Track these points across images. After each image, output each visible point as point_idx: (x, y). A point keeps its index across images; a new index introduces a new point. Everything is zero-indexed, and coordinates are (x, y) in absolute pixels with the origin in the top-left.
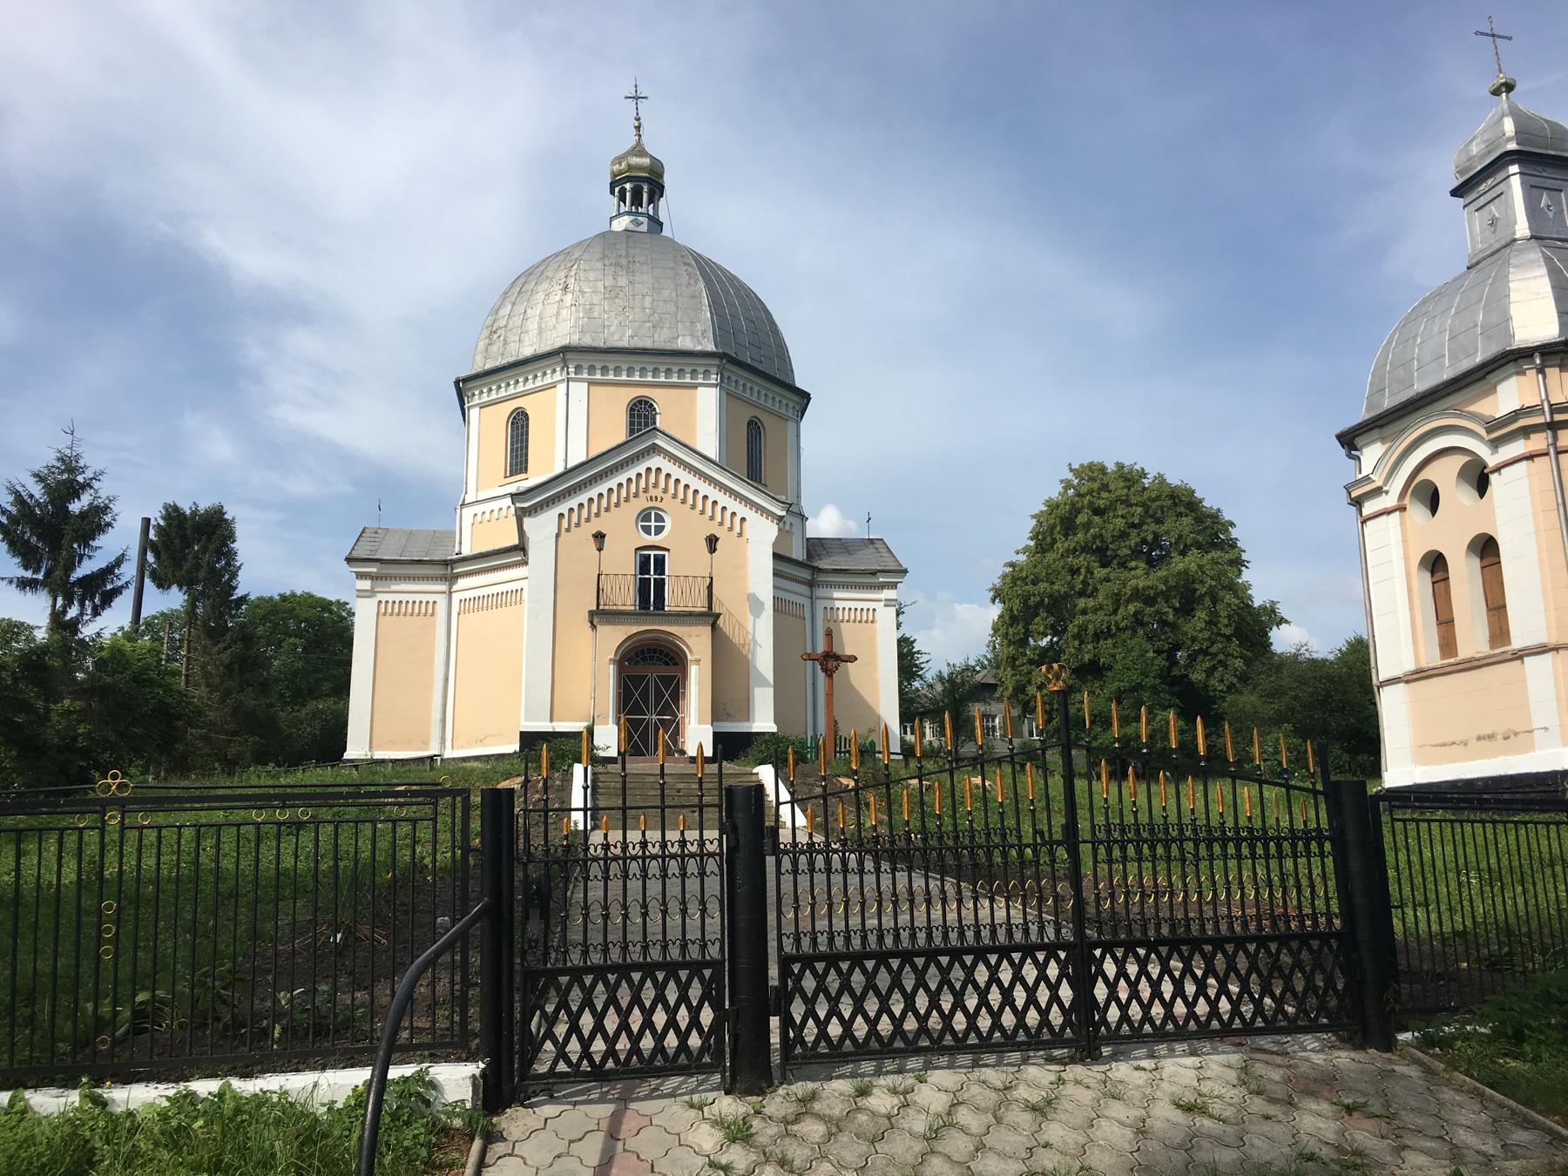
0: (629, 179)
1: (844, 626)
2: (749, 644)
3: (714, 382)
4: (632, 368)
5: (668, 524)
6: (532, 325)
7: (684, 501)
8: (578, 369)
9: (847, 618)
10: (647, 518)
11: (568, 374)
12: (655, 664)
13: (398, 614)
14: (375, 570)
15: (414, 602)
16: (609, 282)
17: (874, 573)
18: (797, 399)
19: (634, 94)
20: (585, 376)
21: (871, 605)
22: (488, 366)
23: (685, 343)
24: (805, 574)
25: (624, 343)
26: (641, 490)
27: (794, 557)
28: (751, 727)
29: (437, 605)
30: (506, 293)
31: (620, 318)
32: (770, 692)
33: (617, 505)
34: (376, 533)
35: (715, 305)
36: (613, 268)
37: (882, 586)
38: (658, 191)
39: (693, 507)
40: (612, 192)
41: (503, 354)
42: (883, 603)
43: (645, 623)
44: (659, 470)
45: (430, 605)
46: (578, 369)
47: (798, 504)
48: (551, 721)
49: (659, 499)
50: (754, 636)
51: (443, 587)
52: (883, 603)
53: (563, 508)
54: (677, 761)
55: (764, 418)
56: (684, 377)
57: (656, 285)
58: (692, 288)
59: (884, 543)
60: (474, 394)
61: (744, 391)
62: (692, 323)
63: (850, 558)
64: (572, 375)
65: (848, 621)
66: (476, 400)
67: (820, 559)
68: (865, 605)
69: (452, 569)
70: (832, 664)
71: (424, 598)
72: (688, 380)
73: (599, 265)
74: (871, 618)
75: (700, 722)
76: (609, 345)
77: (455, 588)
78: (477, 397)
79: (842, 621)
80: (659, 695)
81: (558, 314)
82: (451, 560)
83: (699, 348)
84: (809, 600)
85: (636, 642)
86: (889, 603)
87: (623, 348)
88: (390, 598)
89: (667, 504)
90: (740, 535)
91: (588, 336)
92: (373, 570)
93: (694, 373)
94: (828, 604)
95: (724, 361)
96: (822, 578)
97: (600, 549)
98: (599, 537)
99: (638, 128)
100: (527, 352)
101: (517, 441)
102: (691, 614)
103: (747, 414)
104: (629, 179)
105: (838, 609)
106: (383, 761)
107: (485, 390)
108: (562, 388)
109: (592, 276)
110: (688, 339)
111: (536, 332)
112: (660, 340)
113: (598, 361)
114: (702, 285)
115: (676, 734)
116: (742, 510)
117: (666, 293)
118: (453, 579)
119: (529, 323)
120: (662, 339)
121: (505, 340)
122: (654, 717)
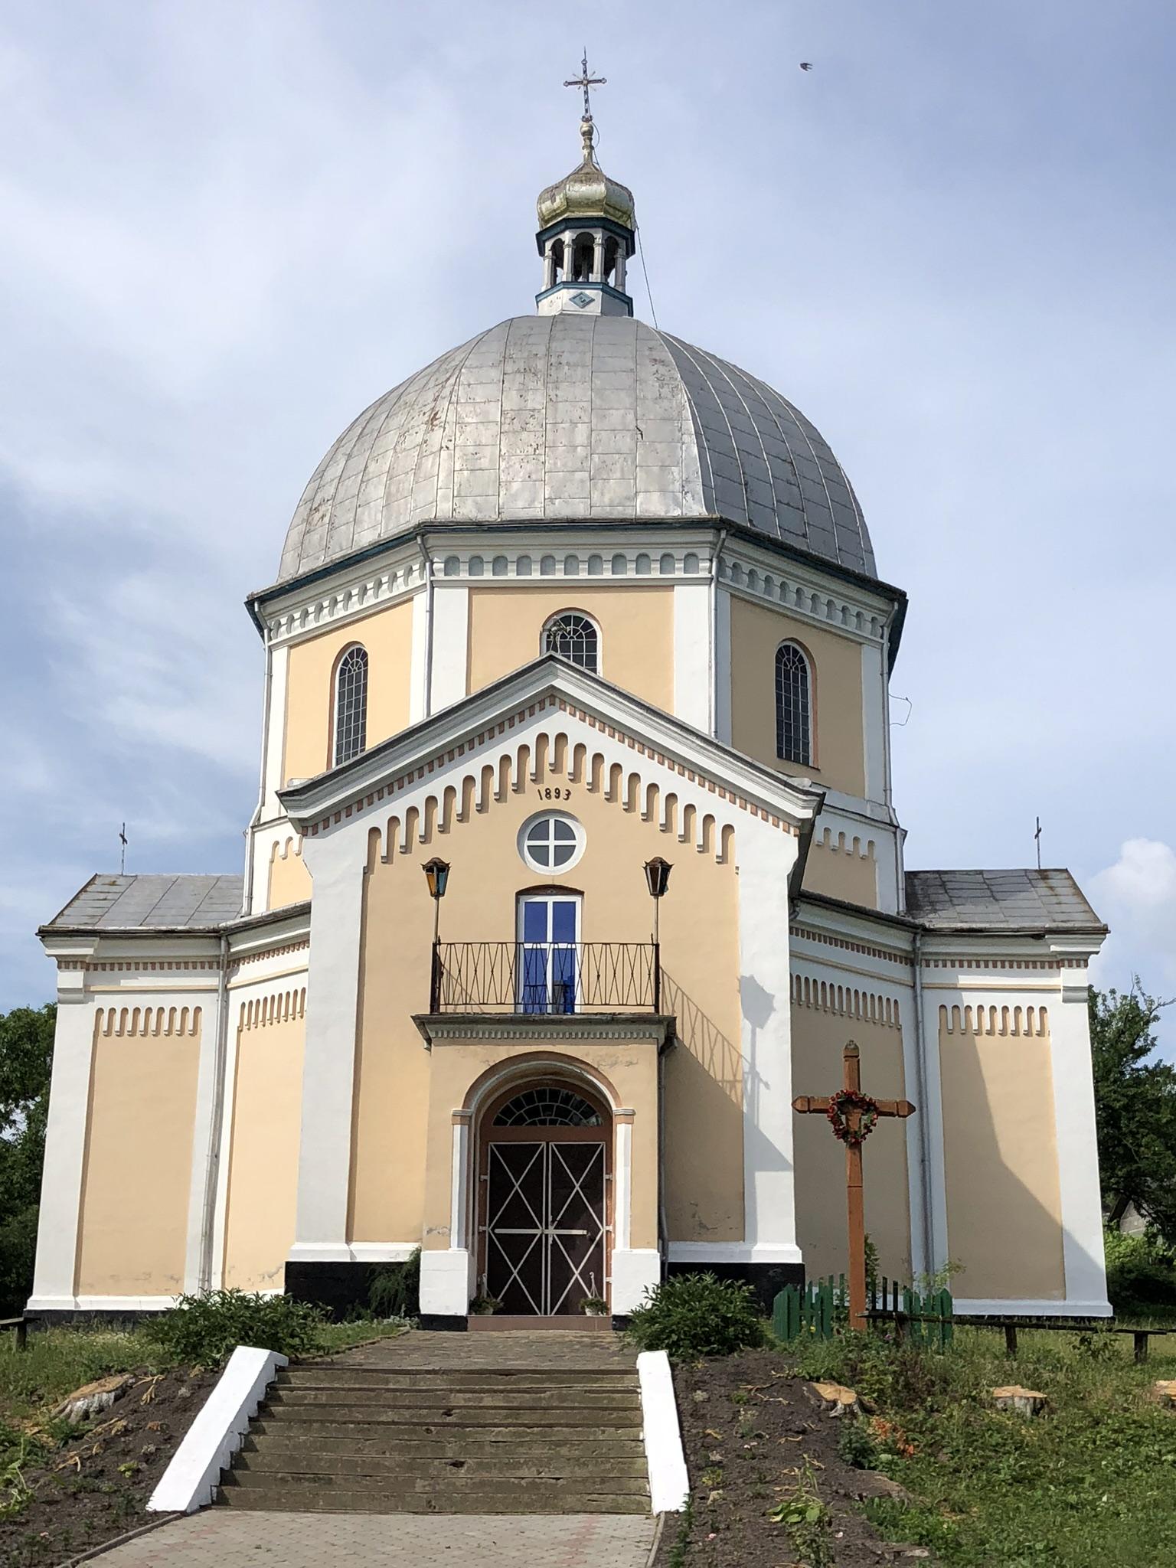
0: (568, 224)
1: (982, 1042)
2: (744, 1081)
3: (706, 575)
4: (574, 557)
5: (581, 842)
6: (376, 491)
7: (611, 797)
8: (451, 563)
9: (987, 1026)
10: (540, 832)
11: (432, 573)
12: (553, 1122)
13: (132, 1033)
14: (90, 951)
15: (161, 1010)
16: (512, 402)
17: (1038, 936)
18: (879, 603)
19: (581, 76)
20: (464, 576)
21: (1036, 1000)
22: (304, 570)
23: (651, 505)
24: (899, 941)
25: (536, 513)
26: (528, 777)
27: (878, 908)
28: (749, 1253)
29: (203, 1015)
30: (340, 440)
31: (529, 467)
32: (787, 1179)
33: (482, 808)
34: (113, 884)
35: (708, 434)
36: (519, 378)
37: (1058, 962)
38: (623, 243)
39: (630, 807)
40: (542, 252)
41: (327, 548)
42: (1059, 996)
43: (524, 1039)
44: (562, 737)
45: (191, 1015)
46: (451, 563)
47: (886, 804)
48: (349, 1239)
49: (563, 794)
50: (753, 1065)
51: (213, 981)
52: (1059, 996)
53: (378, 817)
54: (588, 1325)
55: (811, 641)
56: (673, 570)
57: (598, 402)
58: (665, 404)
59: (1070, 877)
60: (280, 625)
61: (799, 603)
62: (663, 467)
63: (995, 907)
64: (440, 576)
65: (990, 1033)
66: (283, 635)
67: (935, 911)
68: (1024, 1000)
69: (229, 945)
70: (857, 1120)
71: (179, 1001)
72: (656, 574)
73: (495, 374)
74: (1036, 1027)
75: (634, 1243)
76: (506, 516)
77: (235, 981)
78: (283, 629)
79: (978, 1033)
80: (562, 1185)
81: (418, 466)
82: (226, 929)
83: (676, 513)
84: (909, 991)
85: (507, 1081)
86: (1070, 995)
87: (531, 521)
88: (118, 1002)
89: (581, 802)
90: (723, 859)
91: (470, 501)
92: (85, 950)
93: (666, 560)
94: (949, 1001)
95: (723, 534)
96: (933, 947)
97: (438, 894)
98: (437, 870)
99: (588, 134)
100: (366, 538)
101: (349, 706)
102: (613, 1020)
103: (773, 635)
104: (568, 224)
105: (969, 1007)
106: (701, 1268)
107: (297, 615)
108: (421, 600)
109: (480, 393)
110: (656, 496)
111: (381, 502)
112: (605, 502)
113: (488, 546)
114: (683, 397)
115: (597, 1267)
116: (726, 811)
117: (615, 417)
118: (232, 963)
119: (371, 488)
120: (606, 500)
121: (331, 523)
122: (552, 1231)
